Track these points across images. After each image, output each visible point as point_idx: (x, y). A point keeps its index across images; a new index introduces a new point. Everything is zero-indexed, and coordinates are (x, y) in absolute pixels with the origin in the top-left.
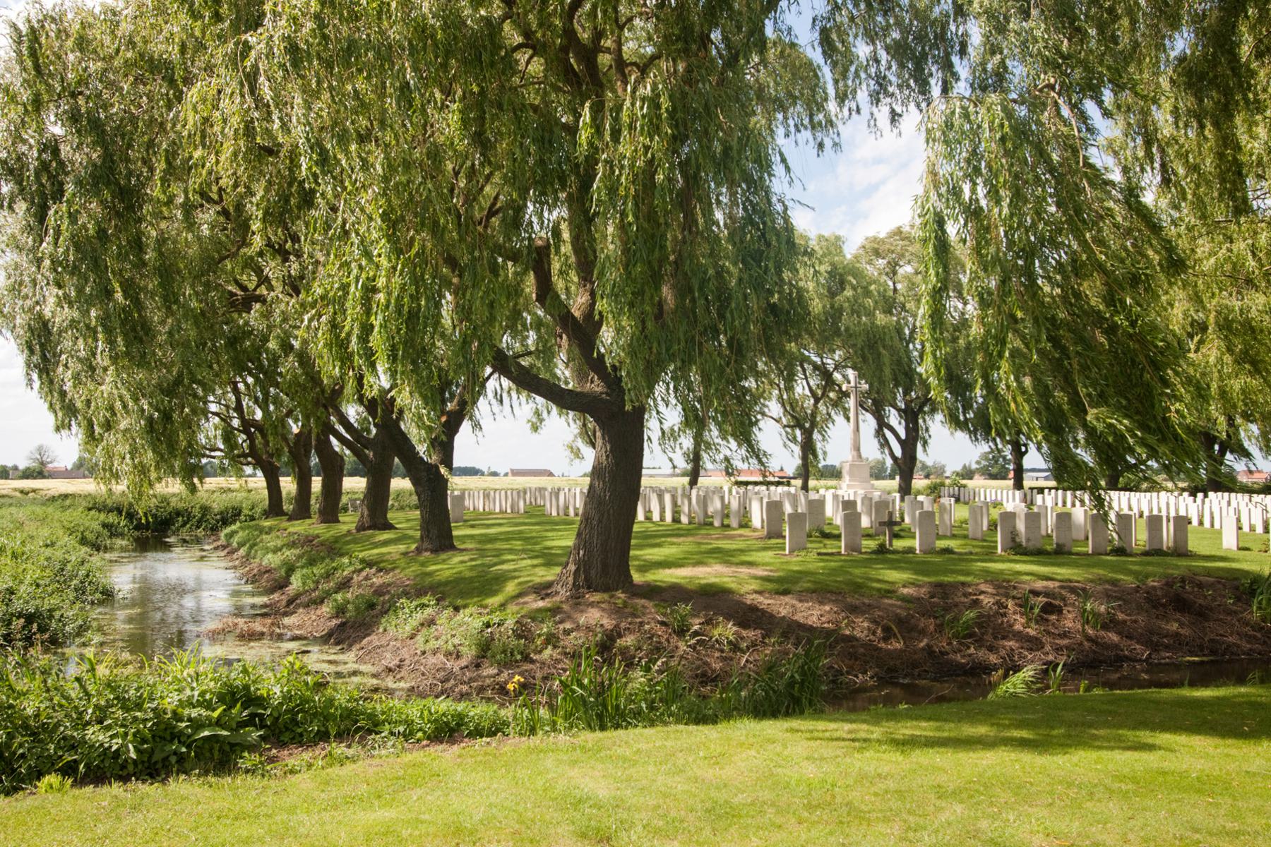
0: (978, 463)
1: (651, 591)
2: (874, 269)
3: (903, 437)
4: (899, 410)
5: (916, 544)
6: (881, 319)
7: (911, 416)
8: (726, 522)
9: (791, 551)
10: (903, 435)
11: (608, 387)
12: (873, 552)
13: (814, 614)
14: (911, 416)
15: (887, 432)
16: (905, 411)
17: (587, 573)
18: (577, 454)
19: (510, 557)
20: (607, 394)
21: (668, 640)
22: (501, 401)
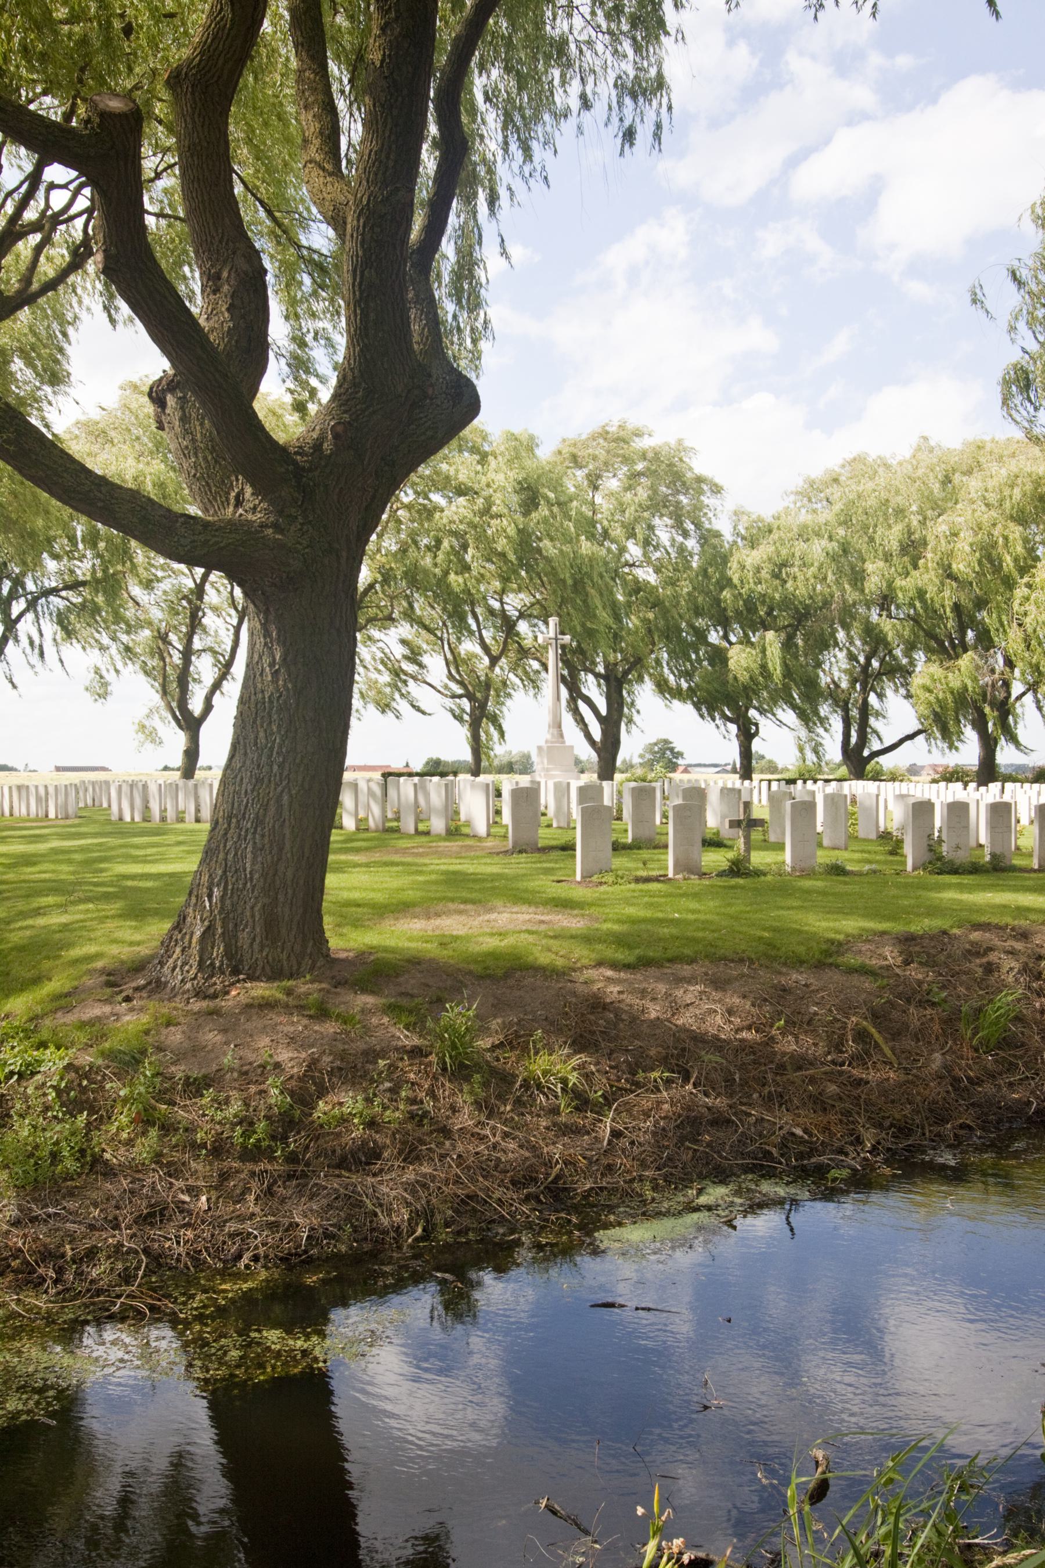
0: (641, 756)
1: (375, 972)
2: (574, 480)
3: (604, 712)
4: (597, 676)
5: (787, 856)
6: (586, 547)
7: (615, 684)
8: (422, 827)
9: (587, 876)
10: (603, 711)
11: (280, 513)
12: (721, 874)
13: (709, 1012)
14: (615, 684)
15: (583, 707)
16: (606, 678)
17: (230, 939)
18: (152, 736)
19: (50, 900)
20: (275, 526)
21: (432, 1093)
22: (42, 654)
